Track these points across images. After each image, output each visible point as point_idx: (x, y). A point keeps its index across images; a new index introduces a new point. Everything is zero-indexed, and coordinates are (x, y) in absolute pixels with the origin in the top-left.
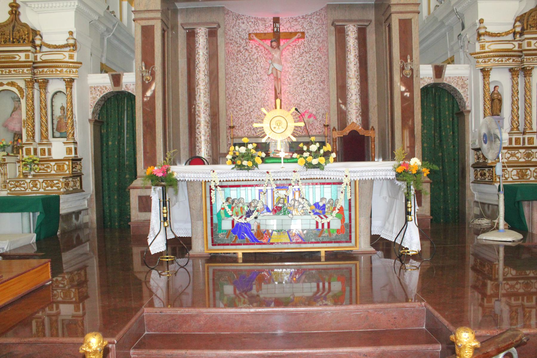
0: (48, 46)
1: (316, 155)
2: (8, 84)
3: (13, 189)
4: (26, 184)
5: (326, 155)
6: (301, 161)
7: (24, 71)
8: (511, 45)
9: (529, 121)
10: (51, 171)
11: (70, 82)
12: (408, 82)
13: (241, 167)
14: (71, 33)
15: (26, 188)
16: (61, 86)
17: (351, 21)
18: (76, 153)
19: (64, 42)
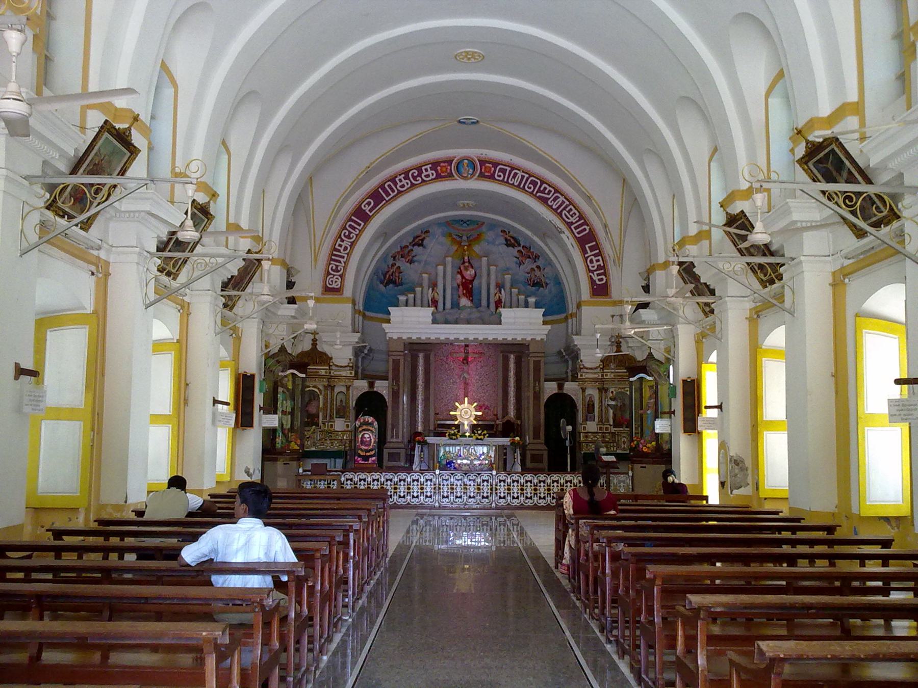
0: (337, 366)
1: (480, 435)
2: (313, 387)
5: (484, 435)
6: (474, 437)
11: (348, 388)
12: (537, 396)
13: (452, 439)
14: (350, 359)
16: (344, 389)
17: (511, 353)
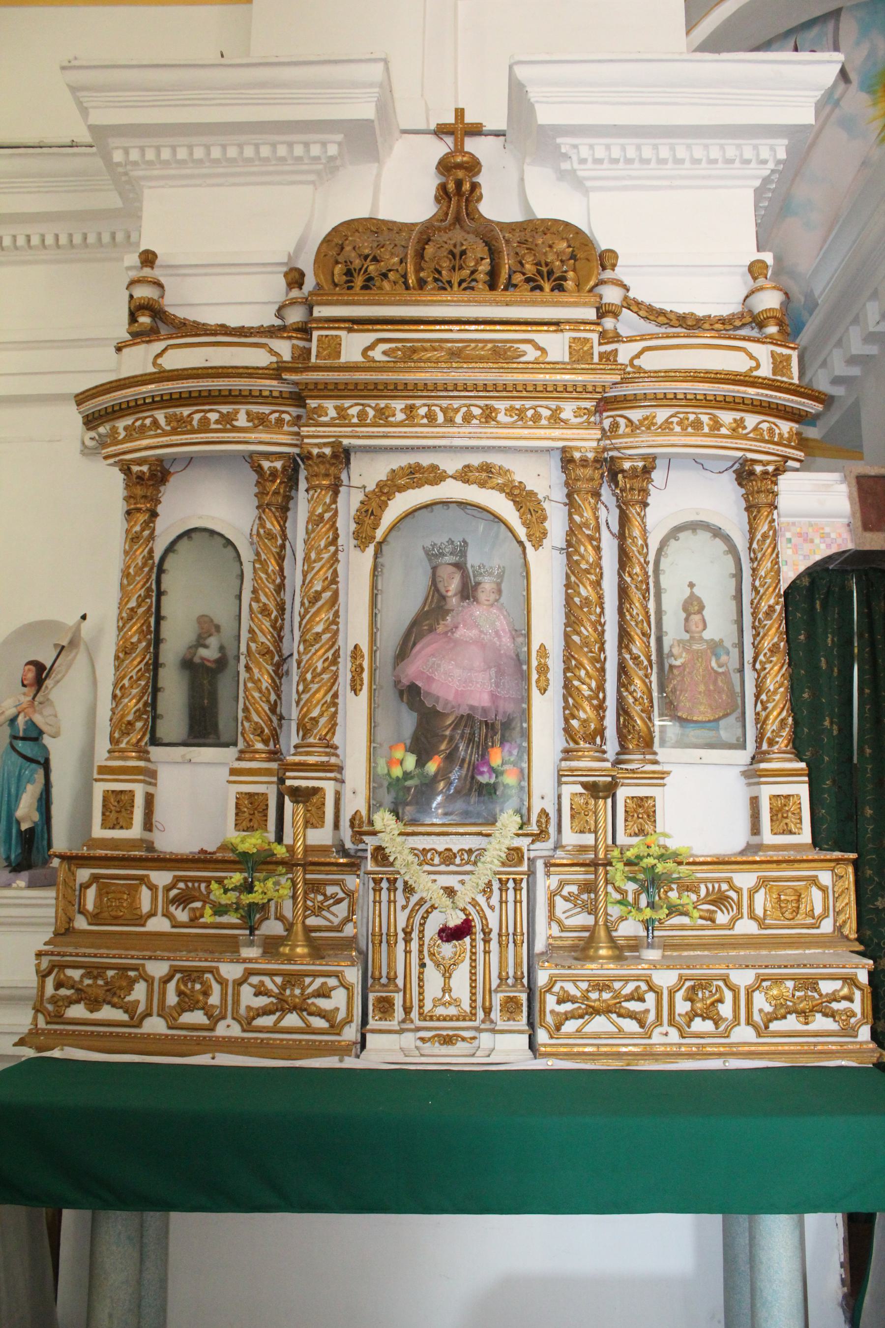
2: (464, 476)
3: (267, 1021)
4: (650, 997)
7: (563, 416)
8: (742, 355)
9: (639, 695)
10: (734, 921)
15: (141, 1008)
18: (148, 825)
19: (269, 319)
